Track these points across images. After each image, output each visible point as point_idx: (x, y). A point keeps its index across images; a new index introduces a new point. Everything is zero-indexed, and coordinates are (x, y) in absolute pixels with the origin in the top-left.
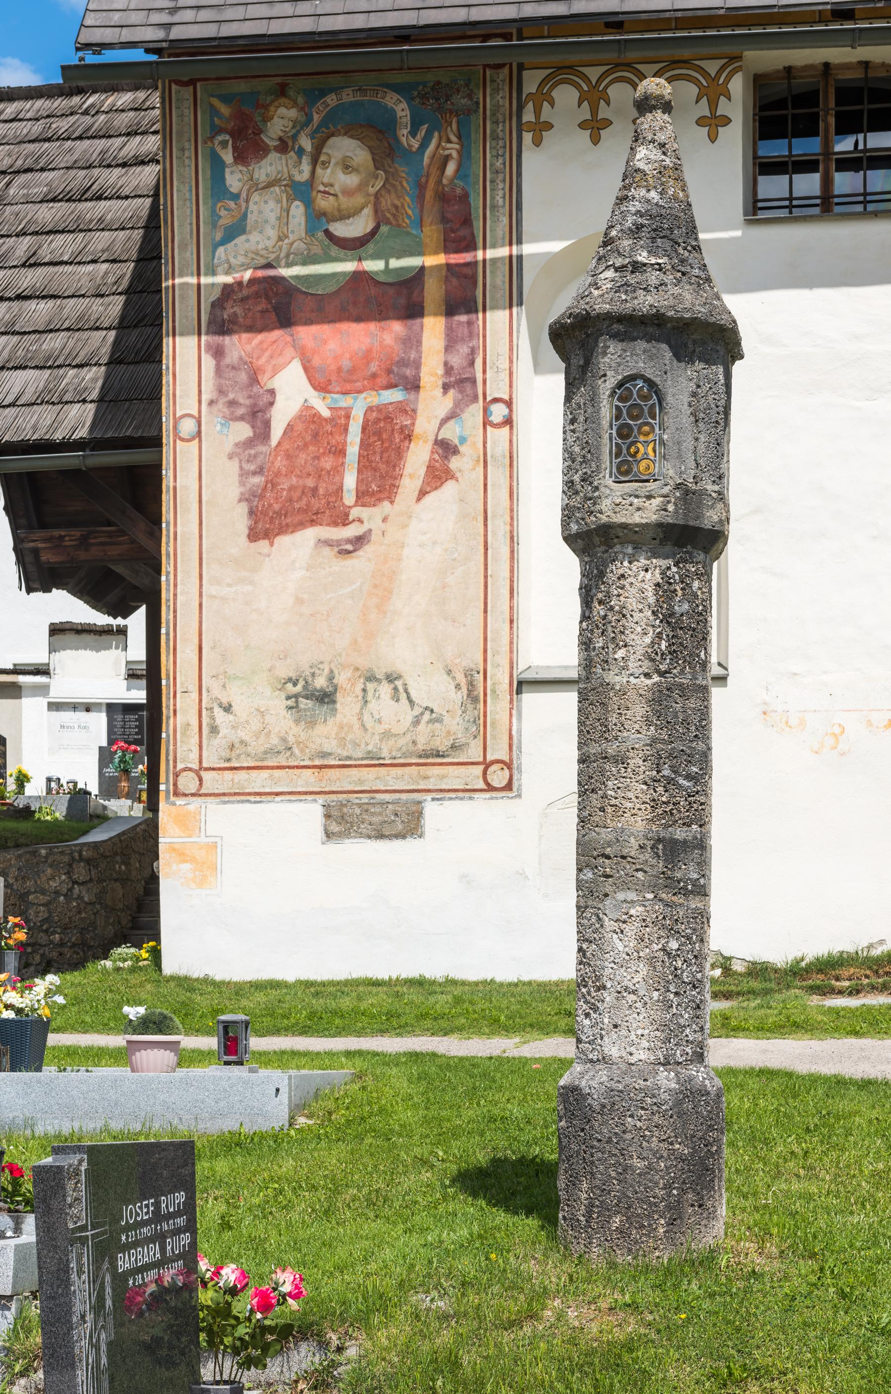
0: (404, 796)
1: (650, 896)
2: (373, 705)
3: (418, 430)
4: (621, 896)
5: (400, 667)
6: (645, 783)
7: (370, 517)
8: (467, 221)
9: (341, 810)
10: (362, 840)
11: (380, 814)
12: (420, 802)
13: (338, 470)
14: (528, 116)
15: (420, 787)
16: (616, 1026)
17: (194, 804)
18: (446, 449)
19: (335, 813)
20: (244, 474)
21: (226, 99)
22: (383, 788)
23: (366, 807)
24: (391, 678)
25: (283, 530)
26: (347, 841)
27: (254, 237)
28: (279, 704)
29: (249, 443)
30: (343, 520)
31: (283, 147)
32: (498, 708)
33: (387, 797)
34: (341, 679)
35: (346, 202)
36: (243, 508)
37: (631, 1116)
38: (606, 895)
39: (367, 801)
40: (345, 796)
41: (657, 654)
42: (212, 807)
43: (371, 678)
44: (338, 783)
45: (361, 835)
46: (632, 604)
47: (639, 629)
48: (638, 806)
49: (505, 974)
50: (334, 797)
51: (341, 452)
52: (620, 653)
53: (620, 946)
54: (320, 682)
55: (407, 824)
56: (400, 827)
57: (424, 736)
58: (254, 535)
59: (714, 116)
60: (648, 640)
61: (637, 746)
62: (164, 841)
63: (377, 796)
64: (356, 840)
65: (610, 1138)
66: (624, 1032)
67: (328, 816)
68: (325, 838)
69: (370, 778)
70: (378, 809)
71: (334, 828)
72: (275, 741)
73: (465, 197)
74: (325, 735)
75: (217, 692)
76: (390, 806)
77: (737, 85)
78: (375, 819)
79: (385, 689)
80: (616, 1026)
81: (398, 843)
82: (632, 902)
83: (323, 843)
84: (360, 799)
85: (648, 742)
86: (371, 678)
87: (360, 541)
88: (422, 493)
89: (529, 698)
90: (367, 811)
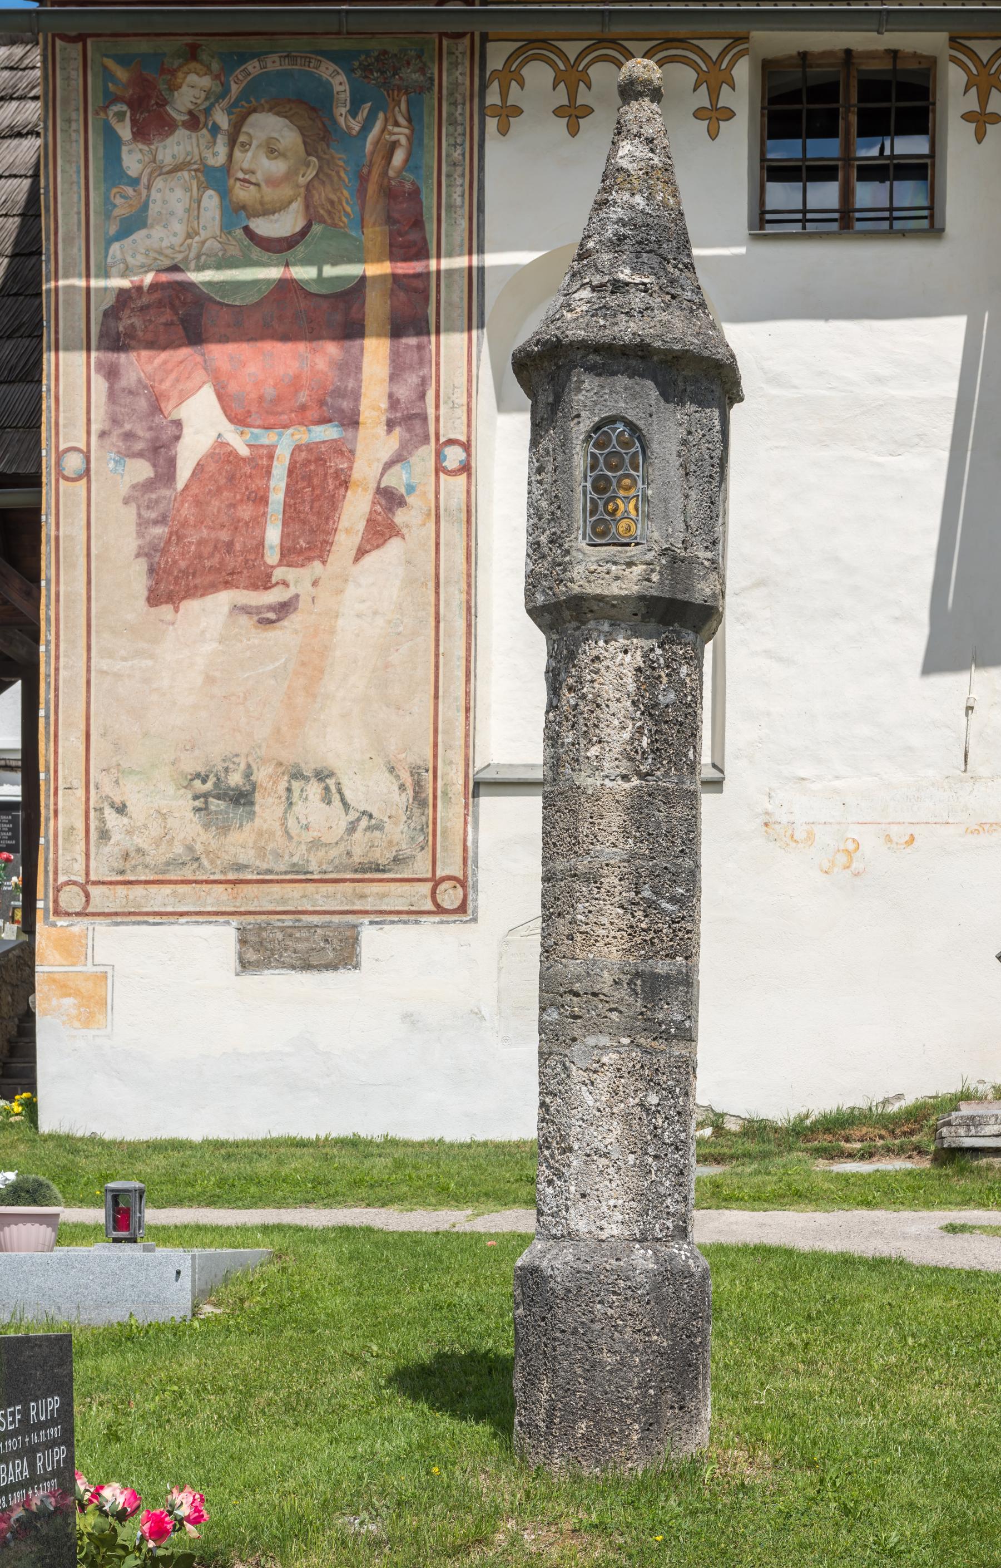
0: (336, 919)
1: (626, 1041)
2: (299, 808)
3: (356, 475)
4: (591, 1041)
5: (333, 762)
6: (622, 907)
7: (298, 580)
8: (418, 223)
9: (259, 935)
10: (284, 971)
11: (307, 940)
12: (355, 926)
13: (259, 521)
15: (355, 908)
16: (584, 1196)
17: (79, 926)
19: (252, 938)
21: (123, 60)
22: (311, 909)
23: (289, 931)
24: (322, 775)
26: (266, 972)
28: (183, 805)
29: (149, 486)
30: (264, 582)
31: (194, 122)
32: (450, 814)
33: (315, 919)
34: (261, 775)
35: (270, 194)
36: (141, 566)
37: (601, 1302)
38: (574, 1040)
39: (291, 924)
40: (264, 917)
41: (637, 752)
43: (297, 775)
44: (256, 903)
45: (284, 965)
46: (608, 691)
47: (616, 722)
48: (613, 933)
50: (251, 919)
51: (262, 499)
52: (594, 751)
53: (590, 1100)
54: (235, 779)
55: (341, 953)
56: (331, 955)
59: (714, 108)
60: (626, 735)
61: (612, 862)
63: (304, 917)
64: (277, 971)
65: (575, 1328)
66: (593, 1203)
67: (243, 942)
68: (239, 969)
69: (295, 896)
70: (304, 934)
71: (251, 956)
72: (179, 849)
74: (240, 844)
75: (108, 789)
76: (319, 931)
77: (743, 72)
78: (301, 946)
80: (584, 1196)
81: (328, 976)
82: (605, 1047)
83: (237, 975)
84: (283, 921)
85: (625, 857)
86: (297, 775)
87: (285, 608)
88: (361, 553)
89: (486, 802)
90: (291, 936)
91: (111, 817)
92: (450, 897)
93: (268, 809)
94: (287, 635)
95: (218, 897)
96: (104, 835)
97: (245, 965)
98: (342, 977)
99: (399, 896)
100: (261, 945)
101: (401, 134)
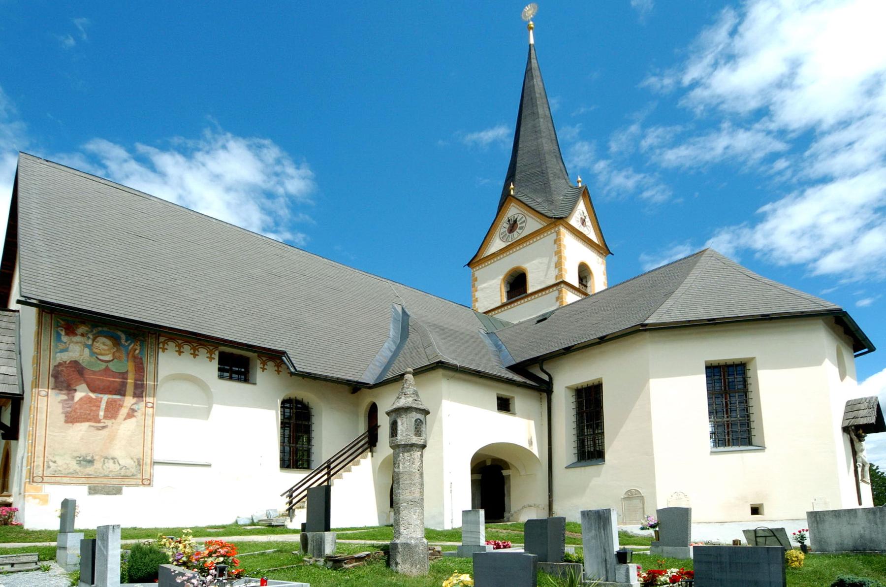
2: (107, 465)
3: (125, 404)
5: (116, 456)
7: (108, 422)
8: (142, 364)
13: (98, 410)
14: (161, 345)
17: (40, 485)
18: (134, 411)
20: (63, 407)
21: (63, 320)
24: (113, 459)
25: (77, 422)
27: (71, 354)
28: (74, 462)
29: (66, 400)
30: (99, 422)
31: (82, 335)
32: (147, 468)
34: (96, 458)
35: (103, 352)
36: (64, 415)
42: (47, 486)
43: (106, 458)
49: (144, 527)
51: (99, 407)
54: (89, 458)
55: (118, 491)
57: (123, 472)
58: (66, 422)
62: (514, 363)
69: (105, 481)
72: (71, 471)
73: (141, 359)
74: (90, 470)
75: (51, 458)
77: (217, 353)
79: (111, 461)
86: (106, 458)
87: (104, 427)
88: (125, 419)
89: (156, 467)
91: (51, 464)
92: (146, 482)
93: (98, 465)
94: (104, 433)
95: (149, 422)
96: (49, 467)
97: (90, 493)
98: (118, 496)
99: (133, 482)
100: (95, 490)
101: (138, 347)
